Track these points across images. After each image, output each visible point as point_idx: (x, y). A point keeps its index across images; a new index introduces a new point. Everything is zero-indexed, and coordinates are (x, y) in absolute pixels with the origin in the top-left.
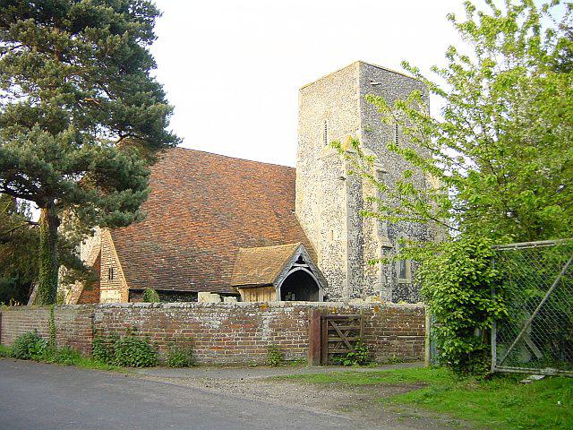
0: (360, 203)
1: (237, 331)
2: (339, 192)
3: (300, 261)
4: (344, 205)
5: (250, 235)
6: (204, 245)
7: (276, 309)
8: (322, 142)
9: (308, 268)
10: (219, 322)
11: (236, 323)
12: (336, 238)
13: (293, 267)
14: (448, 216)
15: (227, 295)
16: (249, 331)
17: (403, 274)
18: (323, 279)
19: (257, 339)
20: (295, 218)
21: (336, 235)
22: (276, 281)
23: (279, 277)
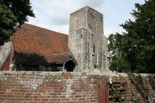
0: (86, 43)
1: (49, 91)
2: (81, 39)
3: (70, 57)
4: (82, 43)
5: (56, 50)
6: (43, 52)
7: (76, 77)
8: (76, 27)
9: (73, 60)
10: (37, 85)
11: (48, 86)
12: (79, 52)
13: (68, 59)
14: (35, 75)
15: (48, 67)
16: (57, 91)
17: (96, 63)
18: (76, 63)
19: (62, 97)
20: (68, 47)
21: (79, 51)
22: (63, 63)
23: (64, 62)
